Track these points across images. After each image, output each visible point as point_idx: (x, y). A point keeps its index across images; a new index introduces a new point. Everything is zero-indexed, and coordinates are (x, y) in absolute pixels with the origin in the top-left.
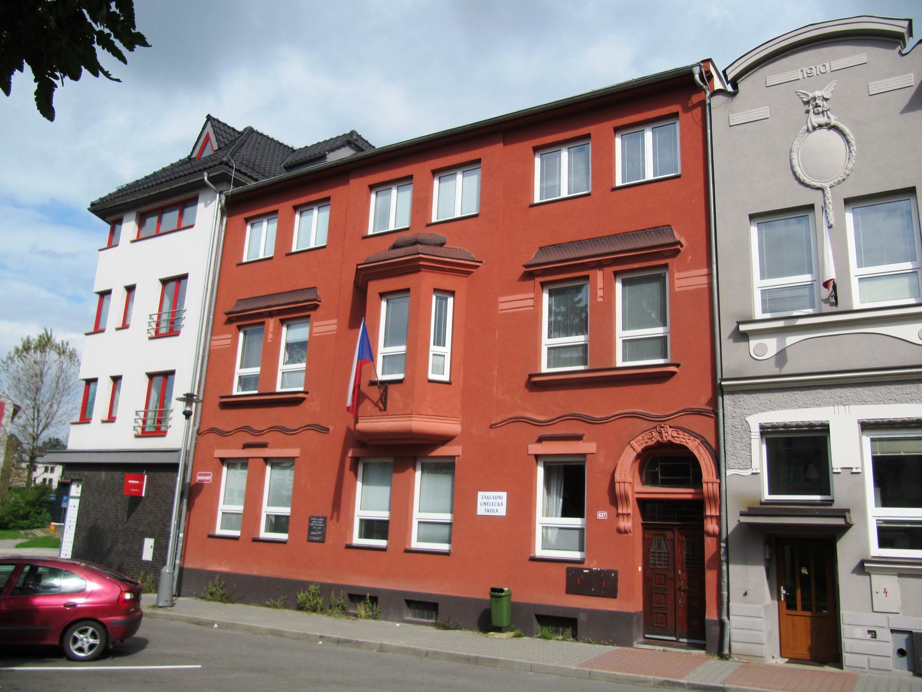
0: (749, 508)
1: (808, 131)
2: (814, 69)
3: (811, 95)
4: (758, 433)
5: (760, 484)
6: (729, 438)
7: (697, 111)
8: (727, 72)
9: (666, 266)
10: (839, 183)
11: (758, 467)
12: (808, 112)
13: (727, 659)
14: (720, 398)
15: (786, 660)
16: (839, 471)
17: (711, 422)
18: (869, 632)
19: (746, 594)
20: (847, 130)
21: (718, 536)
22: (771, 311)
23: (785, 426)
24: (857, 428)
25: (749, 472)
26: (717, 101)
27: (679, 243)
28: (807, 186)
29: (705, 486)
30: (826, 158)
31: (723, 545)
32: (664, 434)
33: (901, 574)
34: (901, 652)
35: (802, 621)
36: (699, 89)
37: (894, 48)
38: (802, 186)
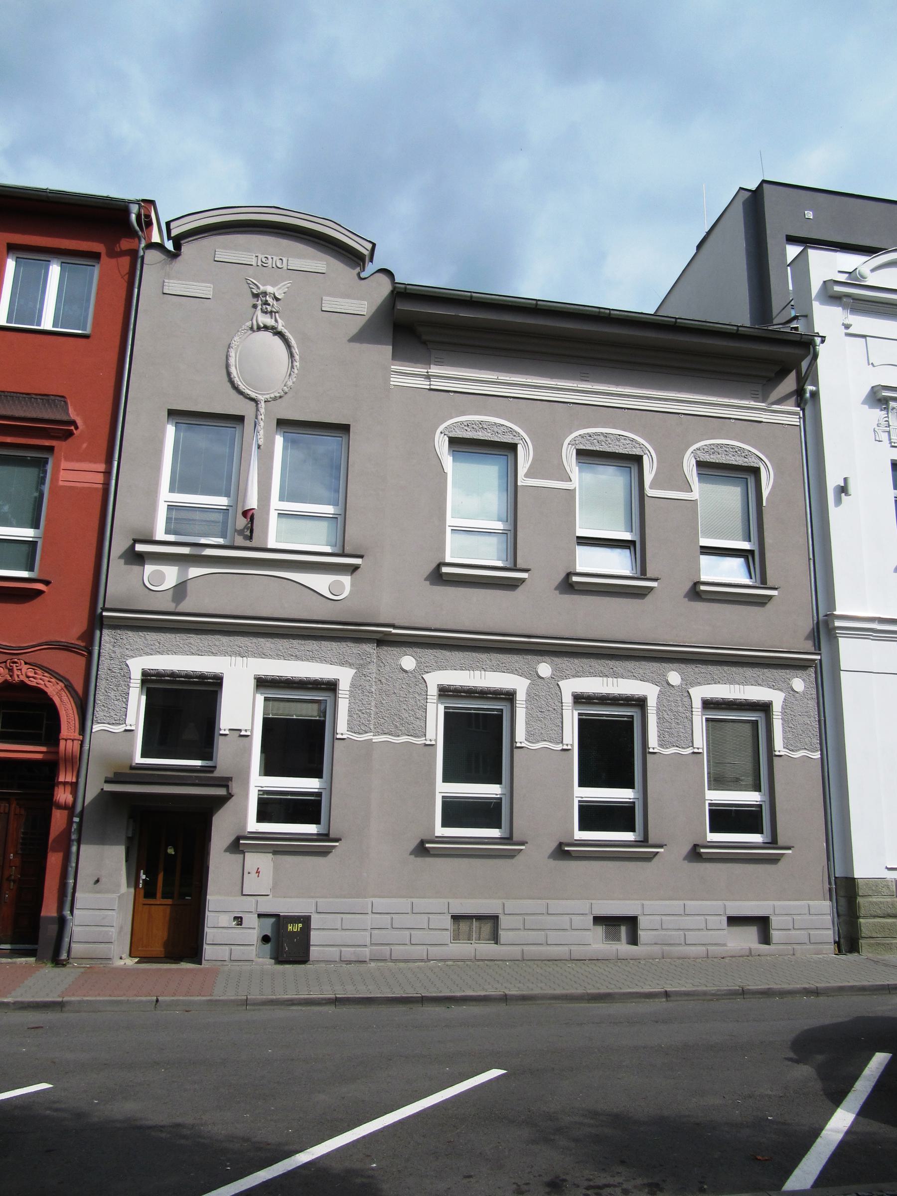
0: (115, 773)
1: (252, 328)
2: (270, 260)
3: (262, 288)
4: (139, 681)
5: (132, 744)
6: (102, 684)
7: (126, 261)
8: (173, 225)
9: (51, 449)
10: (275, 399)
11: (133, 722)
12: (255, 306)
13: (64, 965)
14: (98, 632)
15: (136, 960)
16: (227, 732)
17: (82, 661)
18: (235, 918)
19: (97, 881)
20: (293, 342)
21: (70, 809)
22: (175, 533)
23: (173, 674)
24: (252, 683)
25: (121, 728)
26: (152, 256)
27: (73, 423)
28: (241, 393)
29: (62, 743)
30: (266, 364)
31: (76, 819)
32: (16, 672)
33: (277, 852)
34: (265, 939)
35: (161, 910)
36: (131, 234)
37: (354, 269)
38: (234, 392)
